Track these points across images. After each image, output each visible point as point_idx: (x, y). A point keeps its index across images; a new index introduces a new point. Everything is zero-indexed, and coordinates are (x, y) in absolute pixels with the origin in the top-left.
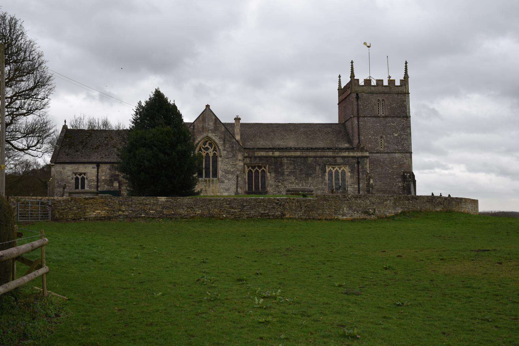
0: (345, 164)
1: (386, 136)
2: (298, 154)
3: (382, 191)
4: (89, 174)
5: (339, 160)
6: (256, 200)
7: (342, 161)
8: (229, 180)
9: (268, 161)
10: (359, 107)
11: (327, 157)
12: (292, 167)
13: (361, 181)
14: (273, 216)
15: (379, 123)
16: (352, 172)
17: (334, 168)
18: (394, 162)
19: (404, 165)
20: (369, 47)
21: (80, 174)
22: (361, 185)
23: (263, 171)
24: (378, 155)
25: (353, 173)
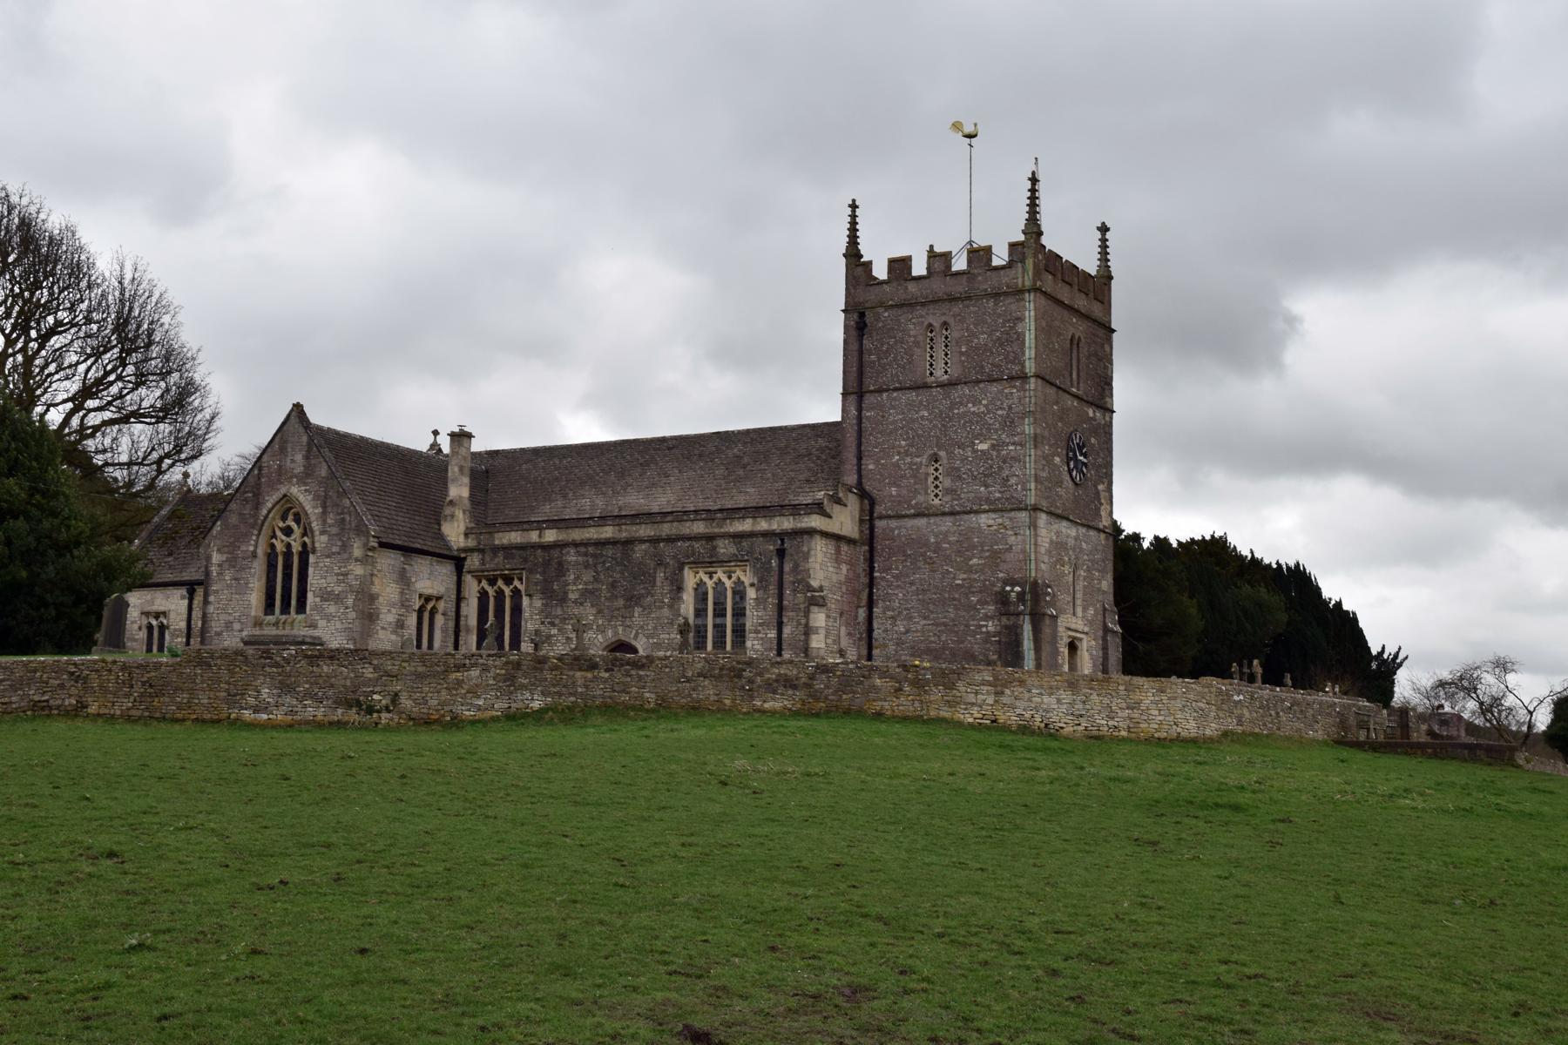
0: (739, 560)
1: (950, 454)
2: (608, 532)
3: (928, 651)
4: (172, 616)
5: (725, 548)
6: (25, 664)
7: (732, 550)
8: (329, 618)
9: (525, 560)
10: (866, 357)
11: (689, 538)
12: (588, 576)
13: (788, 615)
14: (58, 707)
15: (926, 407)
16: (761, 585)
17: (711, 576)
18: (974, 547)
19: (1009, 556)
20: (970, 136)
21: (157, 615)
22: (787, 630)
23: (516, 592)
24: (922, 522)
25: (765, 589)
